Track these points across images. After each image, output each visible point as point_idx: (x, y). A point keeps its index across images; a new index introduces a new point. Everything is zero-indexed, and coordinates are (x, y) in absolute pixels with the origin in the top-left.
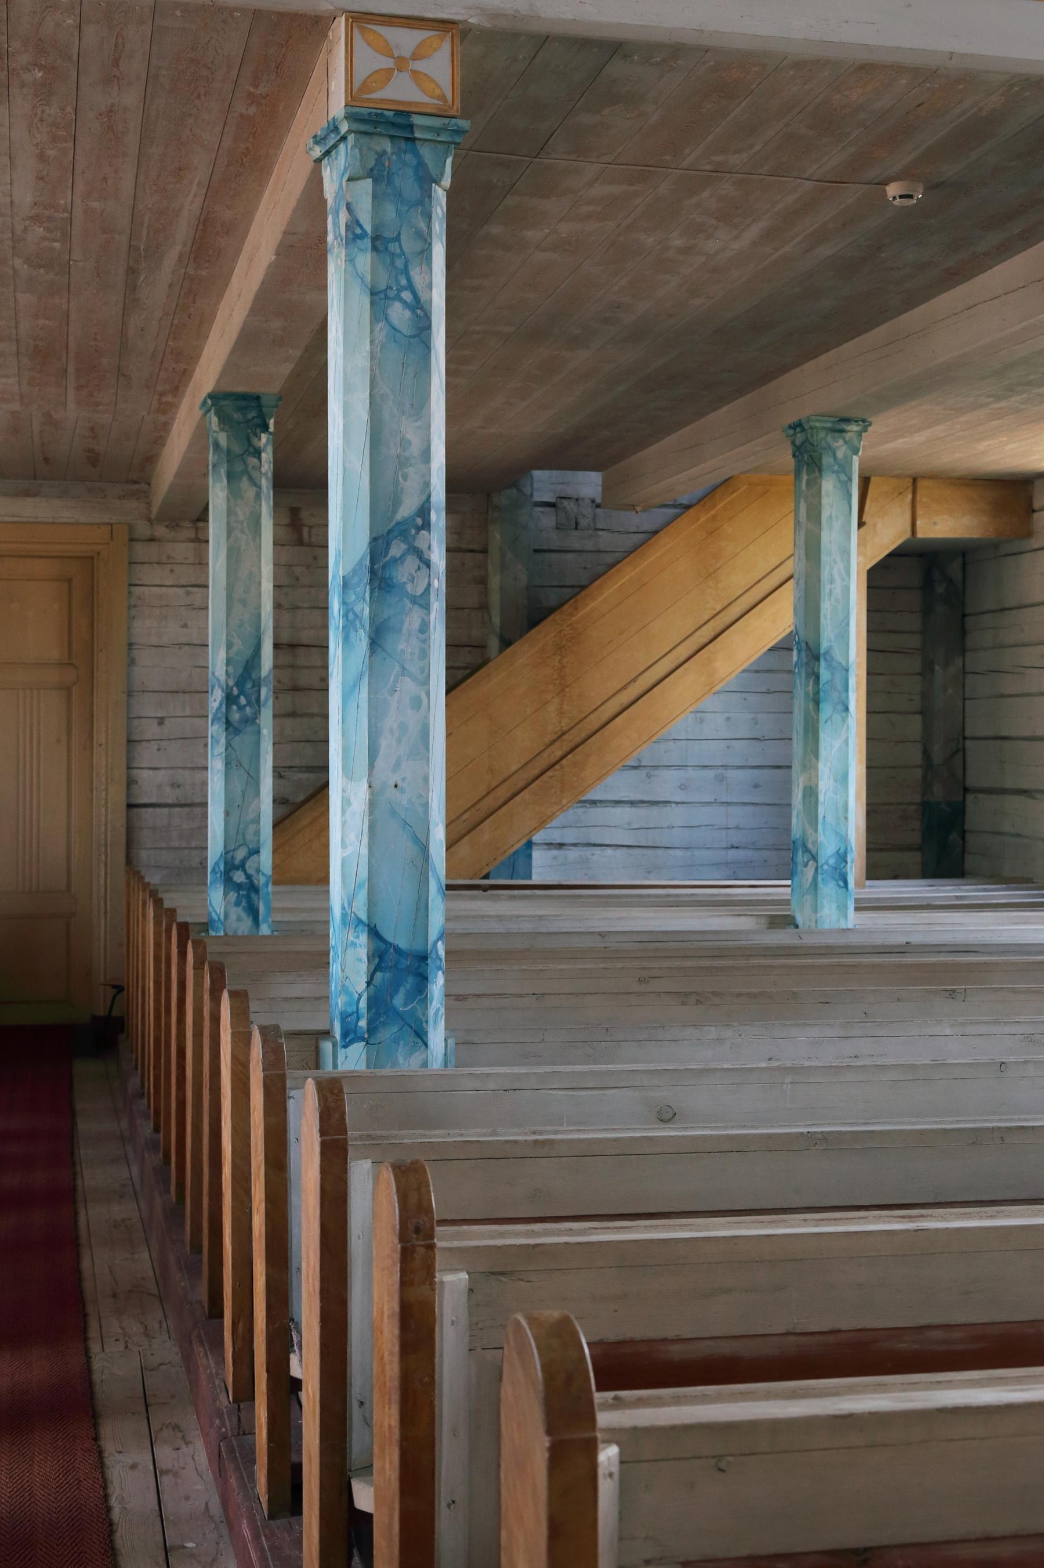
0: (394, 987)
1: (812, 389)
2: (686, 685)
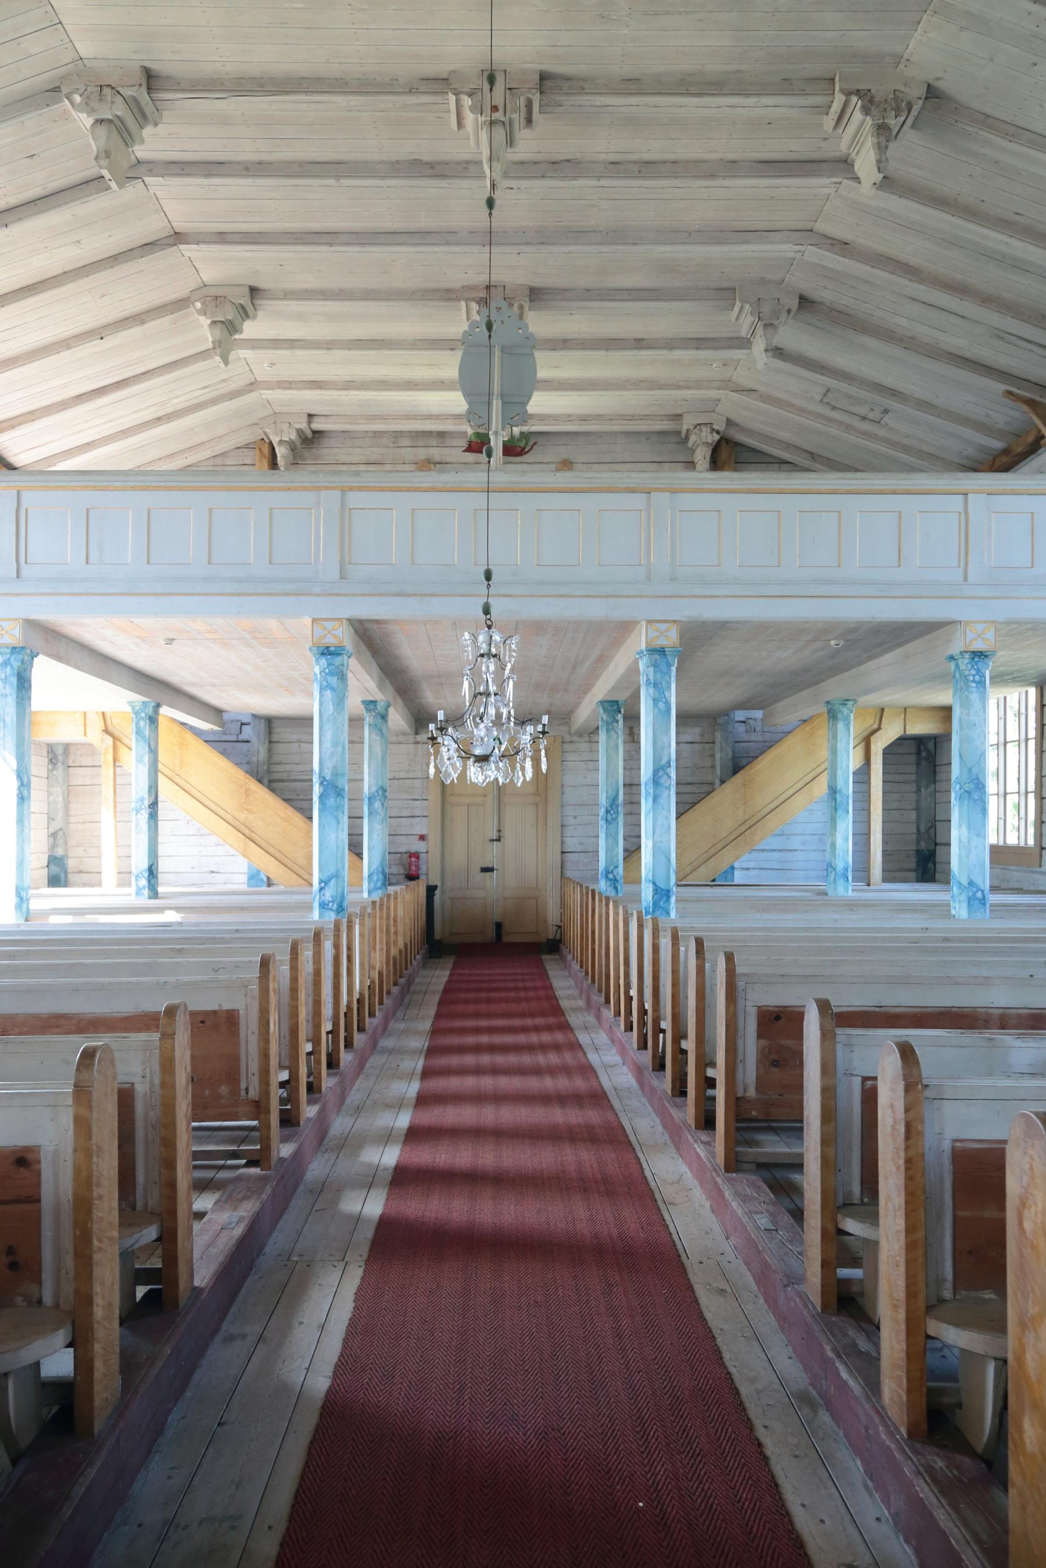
0: (660, 899)
1: (834, 688)
2: (800, 800)
